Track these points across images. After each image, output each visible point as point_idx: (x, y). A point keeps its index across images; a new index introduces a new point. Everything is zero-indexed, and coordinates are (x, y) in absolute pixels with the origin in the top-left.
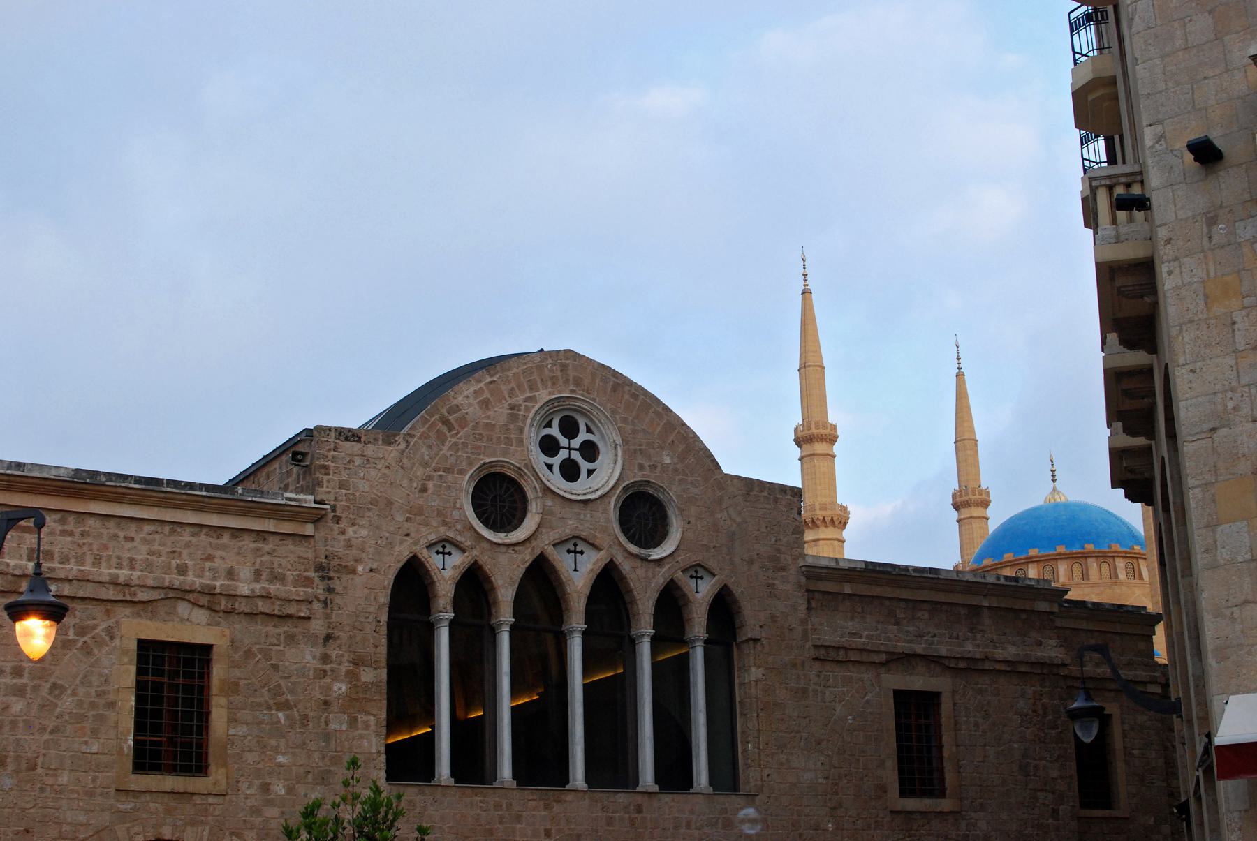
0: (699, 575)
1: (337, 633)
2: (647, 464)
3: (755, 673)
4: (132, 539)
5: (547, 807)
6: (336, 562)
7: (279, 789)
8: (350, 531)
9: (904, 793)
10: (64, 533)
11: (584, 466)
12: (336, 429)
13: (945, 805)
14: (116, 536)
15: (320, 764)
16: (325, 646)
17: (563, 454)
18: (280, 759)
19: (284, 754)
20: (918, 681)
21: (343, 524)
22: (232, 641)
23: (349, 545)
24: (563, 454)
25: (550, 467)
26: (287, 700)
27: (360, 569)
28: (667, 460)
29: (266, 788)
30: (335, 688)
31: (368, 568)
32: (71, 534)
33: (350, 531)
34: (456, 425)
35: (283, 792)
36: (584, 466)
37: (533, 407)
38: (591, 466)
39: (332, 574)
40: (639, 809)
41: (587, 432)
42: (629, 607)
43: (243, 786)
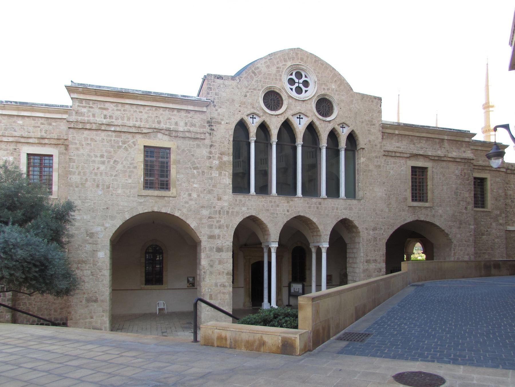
0: (344, 127)
1: (214, 144)
2: (326, 88)
3: (362, 160)
4: (142, 112)
5: (288, 202)
6: (214, 120)
7: (194, 195)
8: (219, 110)
9: (413, 200)
10: (117, 110)
11: (304, 89)
12: (214, 75)
13: (427, 204)
14: (136, 111)
15: (209, 187)
16: (210, 148)
17: (301, 81)
18: (195, 186)
19: (196, 184)
20: (420, 163)
21: (216, 108)
22: (178, 147)
23: (219, 114)
24: (301, 81)
25: (292, 89)
26: (197, 166)
27: (223, 123)
28: (334, 87)
29: (190, 195)
30: (214, 163)
31: (226, 123)
32: (120, 110)
33: (219, 110)
34: (257, 74)
35: (196, 196)
36: (304, 89)
37: (285, 68)
38: (306, 89)
39: (212, 124)
40: (320, 204)
41: (305, 77)
42: (319, 137)
43: (182, 194)
